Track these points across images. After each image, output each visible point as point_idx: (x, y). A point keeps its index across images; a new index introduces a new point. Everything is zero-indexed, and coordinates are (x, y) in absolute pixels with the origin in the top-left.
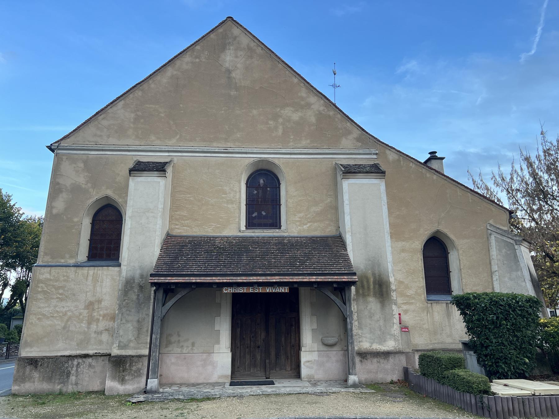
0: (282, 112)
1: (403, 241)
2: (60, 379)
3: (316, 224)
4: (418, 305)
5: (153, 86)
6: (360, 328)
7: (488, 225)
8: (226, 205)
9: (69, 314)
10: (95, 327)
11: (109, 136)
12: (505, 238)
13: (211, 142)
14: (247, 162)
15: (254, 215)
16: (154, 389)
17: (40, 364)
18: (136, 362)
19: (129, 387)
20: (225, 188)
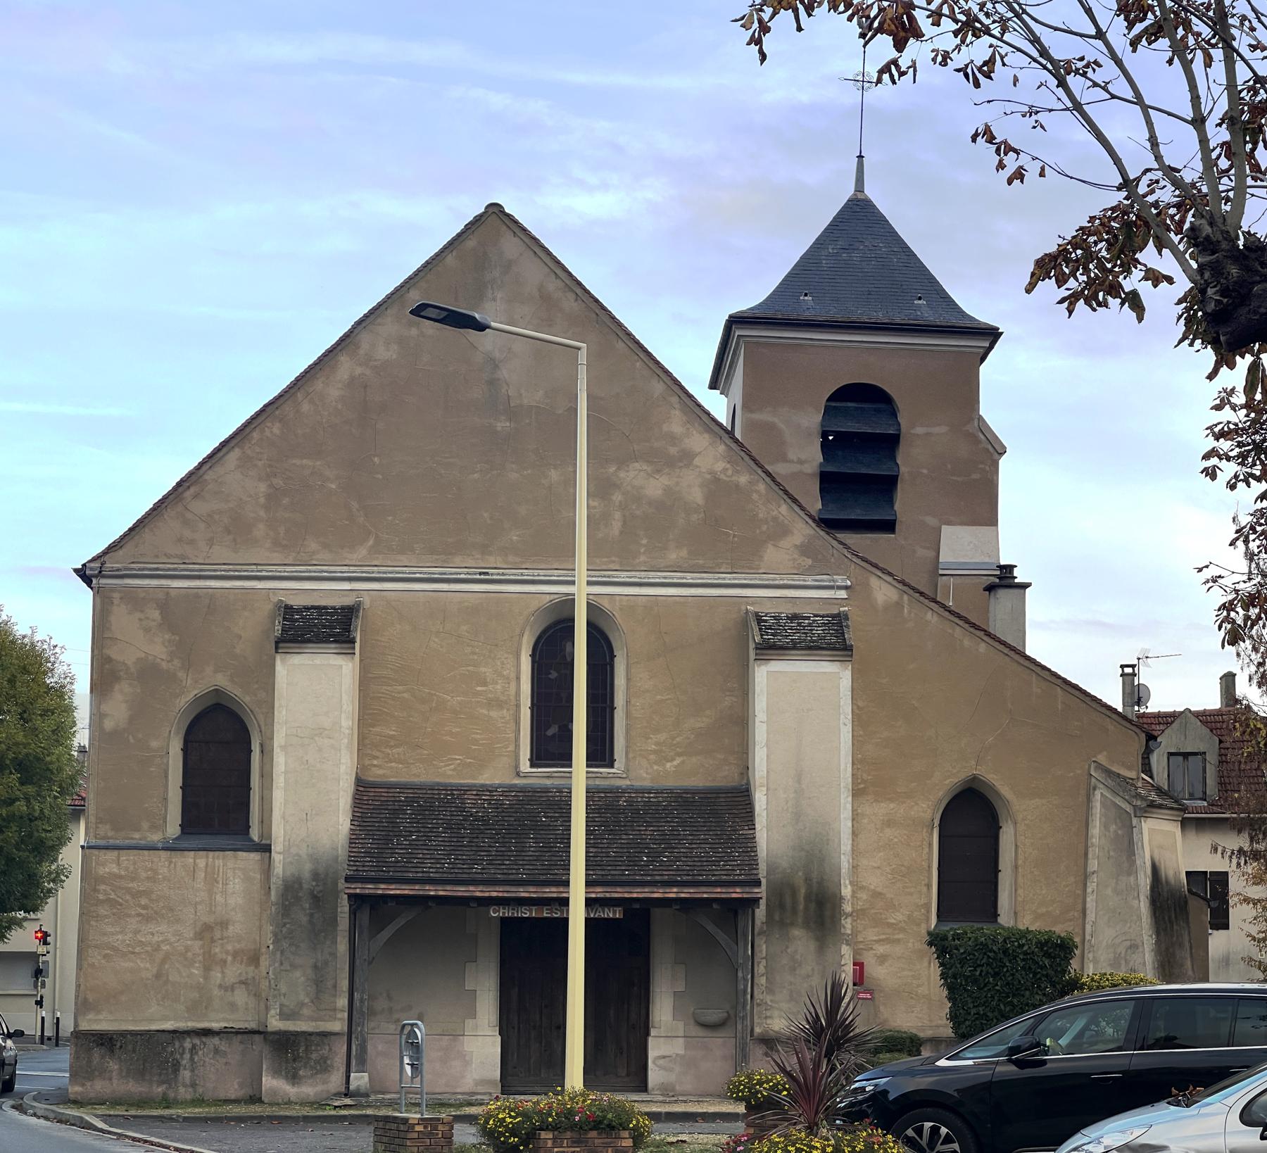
0: (622, 474)
1: (891, 800)
2: (160, 1075)
3: (694, 759)
4: (910, 945)
5: (306, 407)
6: (770, 990)
7: (1093, 765)
8: (485, 712)
9: (165, 948)
10: (219, 975)
11: (211, 542)
12: (1118, 801)
13: (451, 554)
14: (535, 604)
15: (550, 732)
16: (363, 1090)
17: (119, 1044)
18: (317, 1045)
19: (309, 1090)
20: (483, 669)
